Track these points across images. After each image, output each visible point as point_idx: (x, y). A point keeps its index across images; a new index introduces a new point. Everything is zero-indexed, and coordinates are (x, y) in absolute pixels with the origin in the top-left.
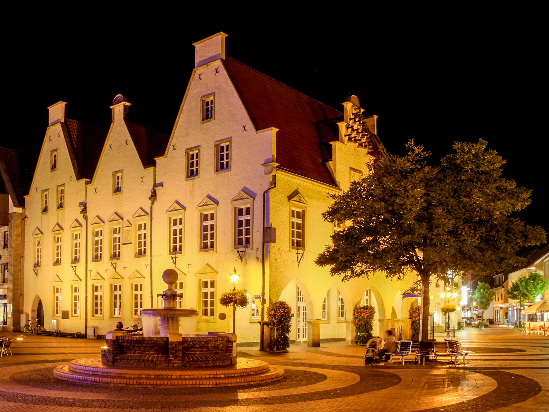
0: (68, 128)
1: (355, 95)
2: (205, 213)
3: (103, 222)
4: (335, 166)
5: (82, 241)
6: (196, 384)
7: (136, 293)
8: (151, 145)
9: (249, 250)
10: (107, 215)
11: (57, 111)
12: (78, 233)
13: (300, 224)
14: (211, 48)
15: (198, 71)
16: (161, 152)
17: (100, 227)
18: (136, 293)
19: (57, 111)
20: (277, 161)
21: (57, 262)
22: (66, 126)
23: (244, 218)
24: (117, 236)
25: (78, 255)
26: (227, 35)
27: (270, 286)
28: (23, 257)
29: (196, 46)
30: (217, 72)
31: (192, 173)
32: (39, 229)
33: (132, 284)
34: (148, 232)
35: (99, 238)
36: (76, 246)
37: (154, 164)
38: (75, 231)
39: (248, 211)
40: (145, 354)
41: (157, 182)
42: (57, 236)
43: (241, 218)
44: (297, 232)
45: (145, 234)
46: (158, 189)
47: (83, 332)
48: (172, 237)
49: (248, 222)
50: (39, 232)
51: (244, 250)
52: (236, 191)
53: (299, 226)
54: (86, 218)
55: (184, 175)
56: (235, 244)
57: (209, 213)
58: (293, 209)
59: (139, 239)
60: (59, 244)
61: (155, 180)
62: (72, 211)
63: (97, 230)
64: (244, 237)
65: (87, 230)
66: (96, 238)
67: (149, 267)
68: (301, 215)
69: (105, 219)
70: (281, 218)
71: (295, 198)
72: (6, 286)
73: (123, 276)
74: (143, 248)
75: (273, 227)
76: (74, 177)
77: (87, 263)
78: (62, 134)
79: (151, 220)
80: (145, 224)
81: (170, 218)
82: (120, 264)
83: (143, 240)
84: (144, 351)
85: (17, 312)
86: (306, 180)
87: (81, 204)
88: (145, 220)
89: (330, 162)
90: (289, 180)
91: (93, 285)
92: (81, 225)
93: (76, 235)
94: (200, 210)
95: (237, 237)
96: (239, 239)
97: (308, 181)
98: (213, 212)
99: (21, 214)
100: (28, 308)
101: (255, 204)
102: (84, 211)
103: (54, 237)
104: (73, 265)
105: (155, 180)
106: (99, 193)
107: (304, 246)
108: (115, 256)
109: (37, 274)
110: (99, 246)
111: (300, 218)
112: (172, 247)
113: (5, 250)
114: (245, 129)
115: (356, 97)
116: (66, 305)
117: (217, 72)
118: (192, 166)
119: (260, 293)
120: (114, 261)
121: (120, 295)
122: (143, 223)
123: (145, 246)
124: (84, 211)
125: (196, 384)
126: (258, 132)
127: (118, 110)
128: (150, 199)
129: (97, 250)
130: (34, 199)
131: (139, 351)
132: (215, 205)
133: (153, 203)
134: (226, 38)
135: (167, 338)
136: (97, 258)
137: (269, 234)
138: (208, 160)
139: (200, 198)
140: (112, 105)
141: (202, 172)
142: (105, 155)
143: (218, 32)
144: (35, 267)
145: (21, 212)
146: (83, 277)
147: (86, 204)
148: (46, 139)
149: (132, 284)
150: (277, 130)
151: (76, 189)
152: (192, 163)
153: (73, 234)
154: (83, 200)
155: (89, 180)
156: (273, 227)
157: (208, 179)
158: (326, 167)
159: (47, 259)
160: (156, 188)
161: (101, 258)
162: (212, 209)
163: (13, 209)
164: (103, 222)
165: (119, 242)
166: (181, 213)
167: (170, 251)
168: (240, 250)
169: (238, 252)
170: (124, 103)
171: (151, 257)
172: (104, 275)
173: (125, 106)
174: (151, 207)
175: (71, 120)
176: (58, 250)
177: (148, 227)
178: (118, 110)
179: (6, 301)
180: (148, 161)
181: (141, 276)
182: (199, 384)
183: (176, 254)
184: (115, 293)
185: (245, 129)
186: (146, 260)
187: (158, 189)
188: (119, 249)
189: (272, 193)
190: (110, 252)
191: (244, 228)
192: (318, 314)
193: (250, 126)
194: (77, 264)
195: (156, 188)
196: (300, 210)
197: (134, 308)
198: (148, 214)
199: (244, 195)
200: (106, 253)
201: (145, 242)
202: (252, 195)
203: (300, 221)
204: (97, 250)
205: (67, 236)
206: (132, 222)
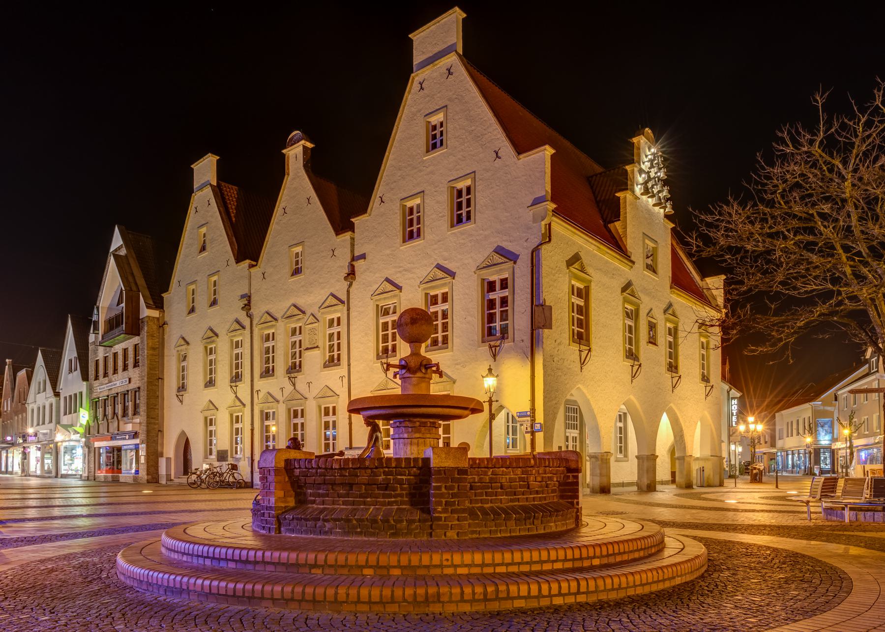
0: (221, 190)
1: (651, 128)
2: (432, 293)
3: (276, 320)
4: (625, 228)
5: (246, 350)
6: (540, 596)
7: (327, 419)
8: (347, 193)
9: (507, 344)
10: (280, 307)
11: (206, 169)
12: (239, 339)
13: (581, 307)
14: (439, 37)
15: (417, 77)
16: (362, 209)
17: (272, 326)
18: (327, 419)
19: (206, 169)
20: (553, 200)
21: (210, 383)
22: (219, 192)
23: (497, 295)
24: (297, 338)
25: (240, 370)
26: (465, 15)
27: (545, 397)
28: (162, 379)
29: (414, 39)
30: (450, 73)
31: (412, 231)
32: (183, 338)
33: (320, 407)
34: (343, 329)
35: (270, 344)
36: (237, 358)
37: (351, 228)
38: (235, 336)
39: (504, 284)
40: (365, 503)
41: (356, 254)
42: (209, 347)
43: (492, 296)
44: (578, 319)
45: (339, 333)
46: (359, 265)
47: (248, 480)
48: (381, 333)
49: (504, 301)
50: (183, 343)
51: (498, 343)
52: (485, 253)
53: (580, 310)
54: (250, 316)
55: (399, 239)
56: (483, 336)
57: (439, 292)
58: (573, 282)
59: (330, 341)
60: (213, 357)
61: (352, 251)
62: (232, 310)
63: (266, 332)
64: (497, 324)
65: (252, 333)
66: (267, 345)
67: (346, 380)
68: (584, 294)
69: (278, 315)
70: (557, 291)
71: (576, 265)
72: (138, 420)
73: (307, 396)
74: (336, 353)
75: (547, 304)
76: (232, 260)
77: (252, 381)
78: (213, 201)
79: (348, 310)
80: (339, 319)
81: (377, 306)
82: (301, 380)
83: (336, 342)
84: (361, 496)
85: (154, 456)
86: (591, 240)
87: (243, 297)
88: (339, 312)
89: (617, 224)
90: (569, 237)
91: (262, 412)
92: (244, 327)
93: (237, 342)
94: (424, 289)
95: (486, 326)
96: (490, 328)
97: (594, 242)
98: (446, 290)
99: (158, 319)
100: (170, 448)
101: (517, 271)
102: (247, 307)
103: (206, 348)
104: (233, 384)
105: (352, 251)
106: (270, 281)
107: (588, 340)
108: (294, 368)
109: (181, 402)
110: (271, 355)
111: (581, 298)
112: (381, 349)
113: (137, 370)
114: (497, 156)
115: (650, 131)
116: (222, 442)
117: (450, 73)
118: (411, 225)
119: (527, 408)
120: (292, 375)
121: (302, 424)
122: (335, 316)
123: (339, 349)
124: (247, 307)
125: (540, 596)
126: (521, 156)
127: (295, 153)
128: (346, 278)
129: (267, 361)
130: (175, 297)
131: (347, 495)
132: (449, 279)
133: (350, 285)
134: (218, 161)
135: (426, 461)
136: (268, 373)
137: (541, 315)
138: (436, 210)
139: (425, 270)
140: (285, 148)
141: (427, 232)
142: (277, 223)
143: (452, 7)
144: (178, 391)
145: (157, 316)
146: (247, 400)
147: (250, 297)
148: (191, 211)
149: (320, 407)
150: (553, 151)
151: (235, 276)
152: (411, 221)
153: (232, 341)
154: (246, 291)
155: (254, 263)
156: (547, 304)
157: (441, 239)
158: (610, 231)
159: (196, 376)
160: (354, 263)
161: (300, 367)
162: (444, 285)
163: (146, 312)
164: (276, 320)
165: (300, 347)
166: (395, 296)
167: (378, 355)
168: (492, 343)
169: (491, 347)
170: (303, 142)
171: (349, 365)
172: (278, 396)
173: (304, 147)
174: (348, 292)
175: (227, 185)
176: (211, 365)
177: (344, 321)
178: (295, 153)
179: (137, 441)
180: (342, 223)
181: (332, 394)
182: (550, 596)
183: (387, 357)
184: (295, 421)
185: (497, 156)
186: (342, 370)
187: (359, 265)
188: (300, 357)
189: (545, 250)
190: (287, 362)
191: (498, 310)
192: (609, 443)
193: (507, 149)
194: (238, 384)
195: (354, 263)
196: (582, 286)
197: (323, 442)
198: (343, 302)
199: (498, 259)
200: (281, 365)
201: (339, 344)
202: (513, 257)
203: (581, 303)
204: (267, 361)
205: (223, 346)
206: (318, 315)
